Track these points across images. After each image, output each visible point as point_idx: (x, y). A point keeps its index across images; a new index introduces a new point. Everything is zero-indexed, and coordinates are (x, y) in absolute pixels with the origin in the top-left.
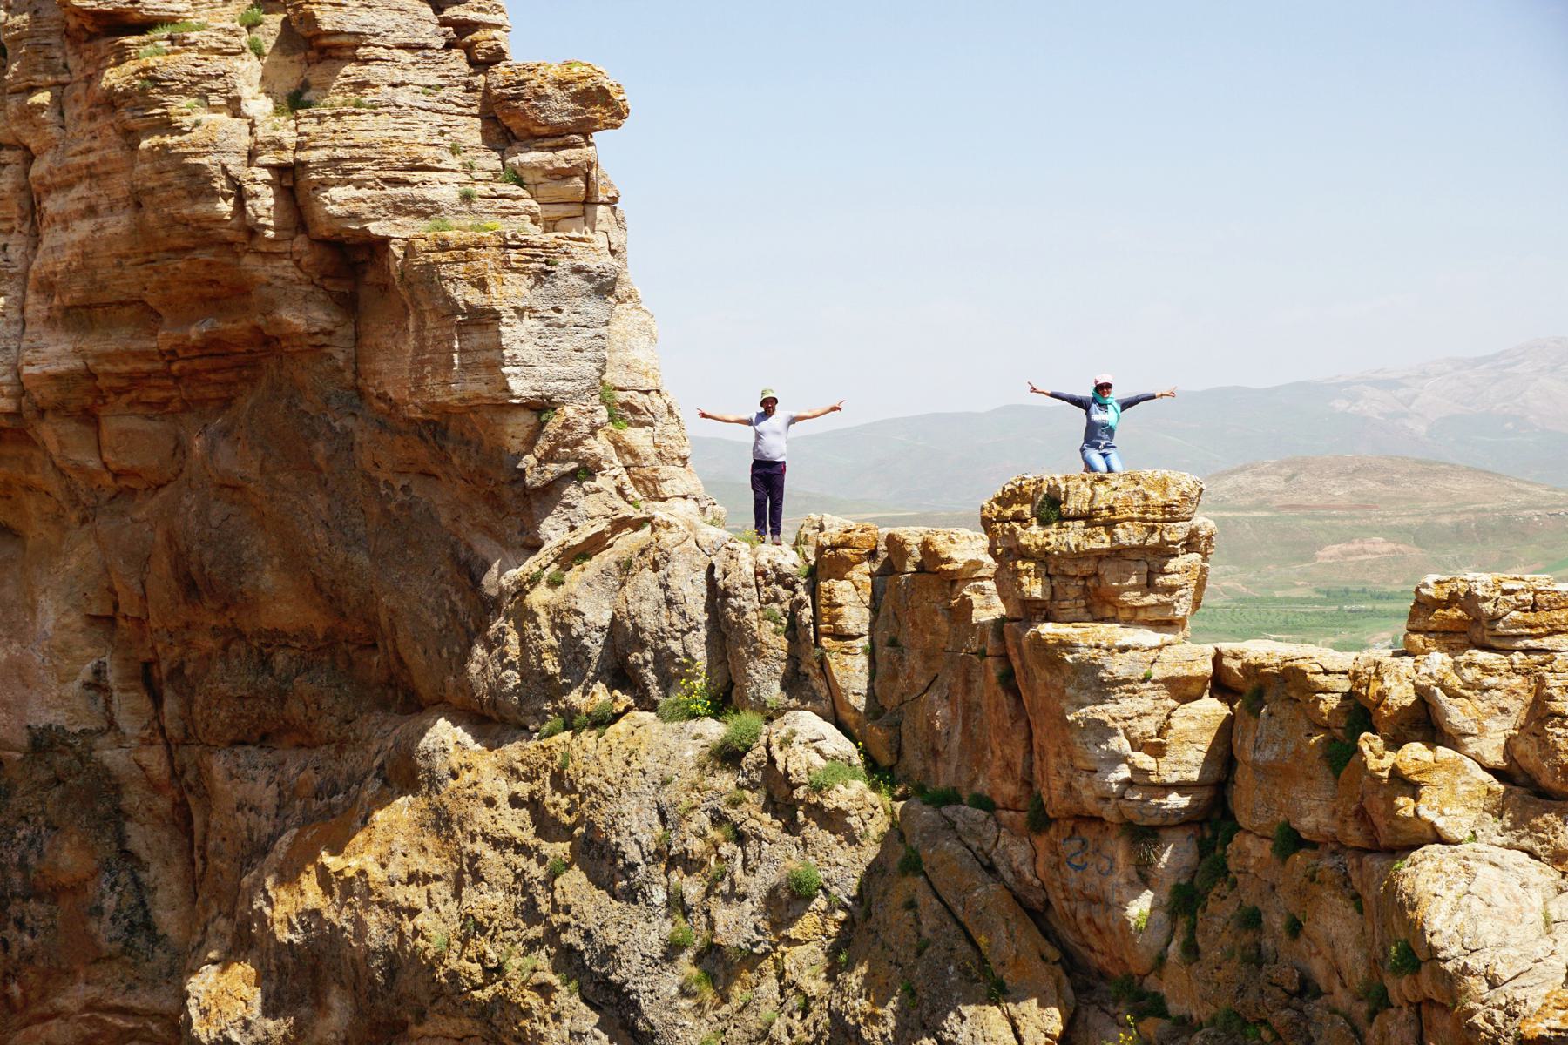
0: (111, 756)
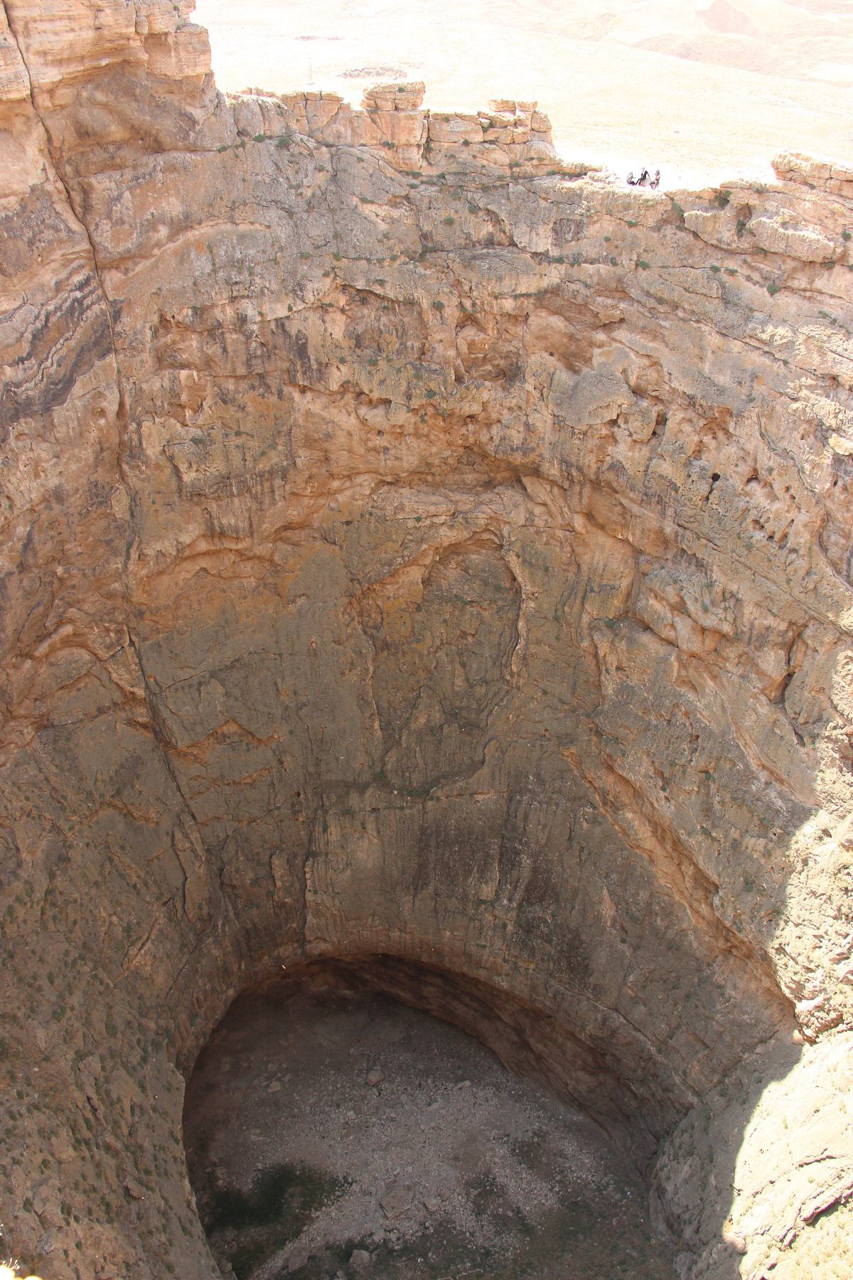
0: (49, 187)
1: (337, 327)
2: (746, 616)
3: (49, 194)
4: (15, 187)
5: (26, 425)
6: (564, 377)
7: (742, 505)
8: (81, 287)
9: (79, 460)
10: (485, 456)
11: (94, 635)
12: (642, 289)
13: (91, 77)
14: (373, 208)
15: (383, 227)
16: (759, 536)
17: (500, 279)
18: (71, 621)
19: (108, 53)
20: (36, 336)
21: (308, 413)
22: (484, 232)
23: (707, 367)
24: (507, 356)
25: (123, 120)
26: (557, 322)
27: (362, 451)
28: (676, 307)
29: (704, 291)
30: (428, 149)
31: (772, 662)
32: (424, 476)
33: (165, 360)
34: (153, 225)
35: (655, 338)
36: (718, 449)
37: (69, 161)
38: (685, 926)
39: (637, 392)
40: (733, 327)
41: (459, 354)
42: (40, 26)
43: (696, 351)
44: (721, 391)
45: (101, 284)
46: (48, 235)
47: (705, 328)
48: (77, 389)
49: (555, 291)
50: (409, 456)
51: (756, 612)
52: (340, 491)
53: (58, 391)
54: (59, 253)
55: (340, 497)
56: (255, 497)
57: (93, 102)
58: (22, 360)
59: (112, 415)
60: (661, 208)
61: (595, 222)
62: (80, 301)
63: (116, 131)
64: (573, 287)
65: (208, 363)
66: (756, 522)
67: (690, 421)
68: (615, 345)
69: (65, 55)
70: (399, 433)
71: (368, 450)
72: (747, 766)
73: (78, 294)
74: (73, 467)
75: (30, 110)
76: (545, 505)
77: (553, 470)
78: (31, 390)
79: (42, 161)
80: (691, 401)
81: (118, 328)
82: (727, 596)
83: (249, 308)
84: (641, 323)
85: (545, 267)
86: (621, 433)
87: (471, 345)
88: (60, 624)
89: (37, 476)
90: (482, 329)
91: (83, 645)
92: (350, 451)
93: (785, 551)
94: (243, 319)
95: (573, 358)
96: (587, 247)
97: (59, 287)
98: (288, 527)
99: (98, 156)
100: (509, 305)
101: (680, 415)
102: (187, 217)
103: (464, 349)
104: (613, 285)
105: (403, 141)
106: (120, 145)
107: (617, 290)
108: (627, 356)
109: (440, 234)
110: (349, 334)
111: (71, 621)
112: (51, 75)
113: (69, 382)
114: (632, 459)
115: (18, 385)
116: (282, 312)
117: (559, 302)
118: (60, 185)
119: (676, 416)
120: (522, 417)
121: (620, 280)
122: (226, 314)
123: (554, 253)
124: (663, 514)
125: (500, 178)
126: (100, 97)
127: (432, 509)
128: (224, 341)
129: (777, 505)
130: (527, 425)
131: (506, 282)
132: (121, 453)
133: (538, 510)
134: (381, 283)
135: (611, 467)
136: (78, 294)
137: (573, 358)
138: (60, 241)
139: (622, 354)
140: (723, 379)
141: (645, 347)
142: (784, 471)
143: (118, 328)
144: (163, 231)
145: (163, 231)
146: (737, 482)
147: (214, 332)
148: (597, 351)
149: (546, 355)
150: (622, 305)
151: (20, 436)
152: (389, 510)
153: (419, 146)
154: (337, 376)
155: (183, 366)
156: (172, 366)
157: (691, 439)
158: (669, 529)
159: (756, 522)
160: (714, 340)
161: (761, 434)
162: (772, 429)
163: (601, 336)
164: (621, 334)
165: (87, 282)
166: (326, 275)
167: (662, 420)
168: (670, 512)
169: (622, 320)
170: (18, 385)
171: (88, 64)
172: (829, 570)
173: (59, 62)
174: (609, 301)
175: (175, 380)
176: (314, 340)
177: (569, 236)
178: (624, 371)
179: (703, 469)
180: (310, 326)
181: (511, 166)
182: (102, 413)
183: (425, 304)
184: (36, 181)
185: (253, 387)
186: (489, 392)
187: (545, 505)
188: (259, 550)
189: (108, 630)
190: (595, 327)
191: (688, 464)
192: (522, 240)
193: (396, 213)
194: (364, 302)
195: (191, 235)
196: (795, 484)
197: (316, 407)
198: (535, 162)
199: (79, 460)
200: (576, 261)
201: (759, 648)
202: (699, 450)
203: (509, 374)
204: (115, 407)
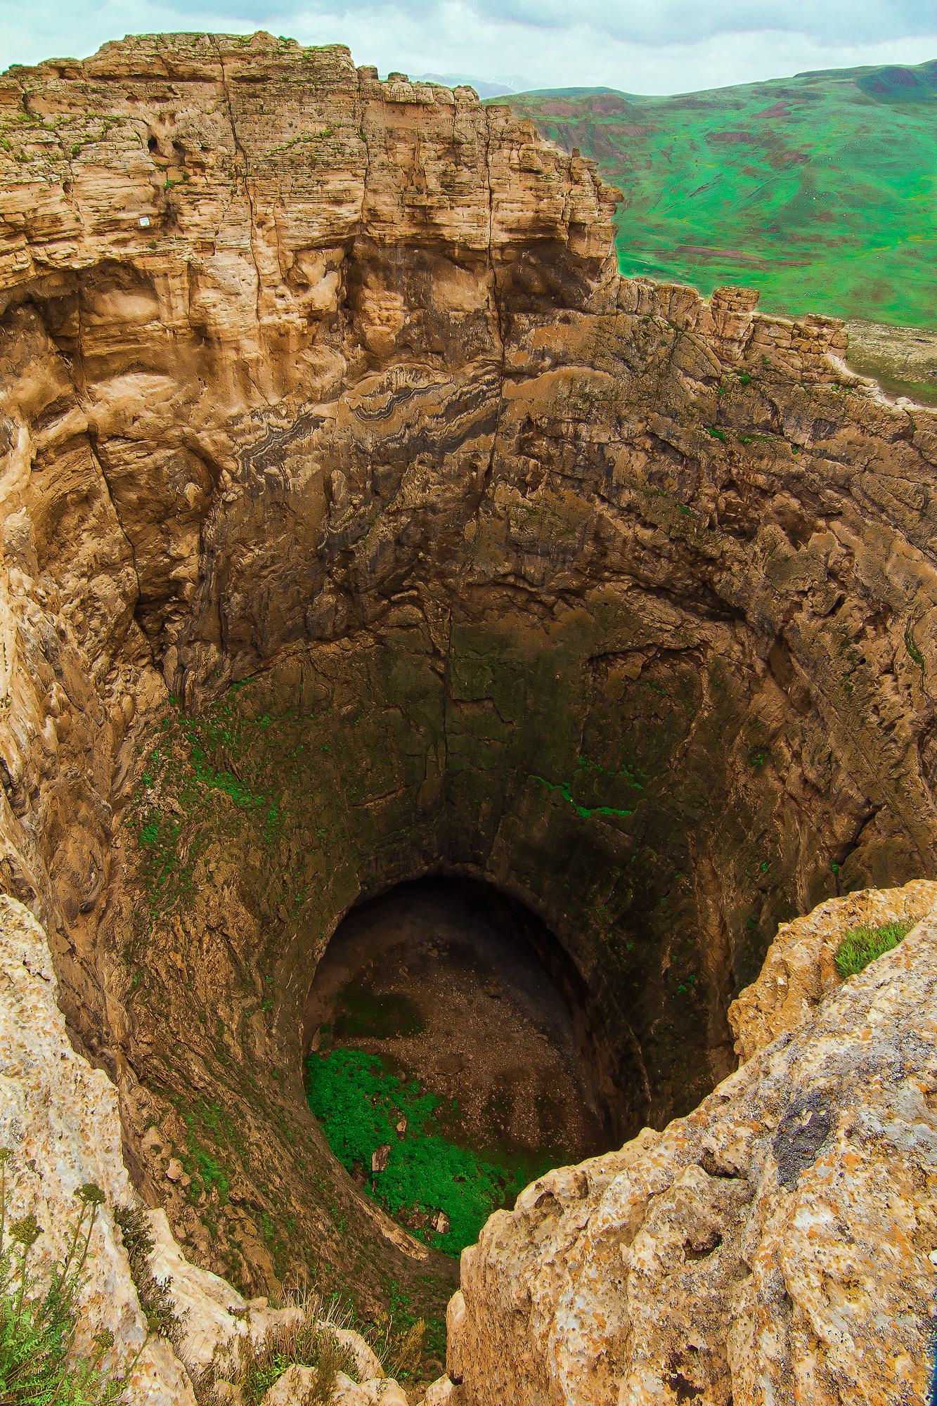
0: (488, 314)
1: (639, 462)
2: (839, 781)
3: (486, 319)
4: (466, 306)
5: (427, 456)
6: (785, 548)
7: (871, 689)
8: (488, 383)
9: (453, 492)
10: (713, 592)
11: (429, 605)
12: (862, 490)
13: (530, 245)
14: (690, 380)
15: (693, 397)
16: (874, 719)
17: (761, 458)
18: (417, 589)
19: (542, 230)
20: (450, 405)
21: (601, 516)
22: (763, 419)
23: (888, 567)
24: (751, 520)
25: (544, 279)
26: (795, 503)
27: (630, 557)
28: (883, 510)
29: (908, 501)
30: (748, 347)
31: (842, 826)
32: (662, 591)
33: (523, 448)
34: (542, 355)
35: (858, 534)
36: (873, 640)
37: (504, 300)
38: (710, 1007)
39: (832, 574)
40: (920, 537)
41: (717, 508)
42: (505, 205)
43: (884, 552)
44: (892, 589)
45: (500, 387)
46: (476, 343)
47: (899, 533)
48: (464, 447)
49: (798, 477)
50: (661, 571)
51: (847, 782)
52: (609, 580)
53: (453, 444)
54: (482, 357)
55: (607, 585)
56: (552, 561)
57: (527, 263)
58: (437, 416)
59: (481, 473)
60: (900, 424)
61: (846, 426)
62: (484, 393)
63: (537, 285)
64: (812, 476)
65: (550, 459)
66: (876, 707)
67: (861, 609)
68: (829, 532)
69: (514, 226)
70: (656, 552)
71: (635, 558)
72: (794, 903)
73: (485, 388)
74: (448, 495)
75: (486, 258)
76: (742, 644)
77: (752, 617)
78: (435, 436)
79: (488, 295)
80: (866, 594)
81: (502, 418)
82: (833, 759)
83: (583, 429)
84: (852, 517)
85: (798, 456)
86: (807, 603)
87: (729, 504)
88: (412, 587)
89: (424, 491)
90: (740, 495)
91: (421, 608)
92: (622, 554)
93: (887, 739)
94: (577, 436)
95: (798, 533)
96: (832, 445)
97: (475, 379)
98: (568, 591)
99: (521, 300)
100: (761, 479)
101: (855, 602)
102: (565, 354)
103: (723, 506)
104: (842, 482)
105: (729, 335)
106: (538, 296)
107: (843, 488)
108: (832, 544)
109: (731, 413)
110: (645, 470)
111: (417, 589)
112: (504, 238)
113: (461, 441)
114: (807, 627)
115: (430, 431)
116: (604, 439)
117: (799, 487)
118: (496, 314)
119: (851, 602)
120: (745, 570)
121: (848, 479)
122: (567, 429)
123: (809, 446)
124: (814, 678)
125: (792, 379)
126: (532, 260)
127: (665, 617)
128: (562, 448)
129: (896, 698)
130: (746, 578)
131: (765, 461)
132: (476, 499)
133: (737, 647)
134: (678, 439)
135: (792, 629)
136: (485, 388)
137: (798, 533)
138: (484, 350)
139: (831, 540)
140: (898, 581)
141: (848, 539)
142: (910, 670)
143: (502, 418)
144: (548, 361)
145: (548, 361)
146: (875, 670)
147: (557, 439)
148: (815, 534)
149: (779, 528)
150: (845, 500)
151: (421, 462)
152: (636, 607)
153: (741, 342)
154: (628, 496)
155: (533, 456)
156: (527, 454)
157: (856, 624)
158: (815, 690)
159: (876, 707)
160: (901, 544)
161: (906, 635)
162: (917, 631)
163: (821, 523)
164: (836, 525)
165: (492, 382)
166: (640, 421)
167: (840, 601)
168: (819, 678)
169: (840, 514)
170: (430, 431)
171: (529, 235)
172: (917, 769)
173: (510, 231)
174: (836, 495)
175: (526, 463)
176: (620, 466)
177: (822, 435)
178: (827, 555)
179: (855, 651)
180: (619, 454)
181: (802, 371)
182: (475, 468)
183: (704, 462)
184: (478, 306)
185: (573, 487)
186: (729, 545)
187: (742, 644)
188: (544, 598)
189: (438, 607)
190: (821, 515)
191: (845, 644)
192: (789, 432)
193: (705, 389)
194: (664, 451)
195: (564, 369)
196: (915, 685)
197: (608, 515)
198: (820, 370)
199: (453, 492)
200: (824, 454)
201: (838, 812)
202: (860, 635)
203: (746, 535)
204: (485, 468)
